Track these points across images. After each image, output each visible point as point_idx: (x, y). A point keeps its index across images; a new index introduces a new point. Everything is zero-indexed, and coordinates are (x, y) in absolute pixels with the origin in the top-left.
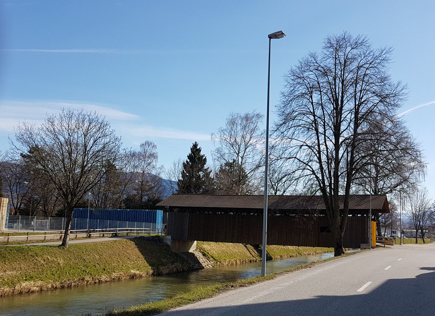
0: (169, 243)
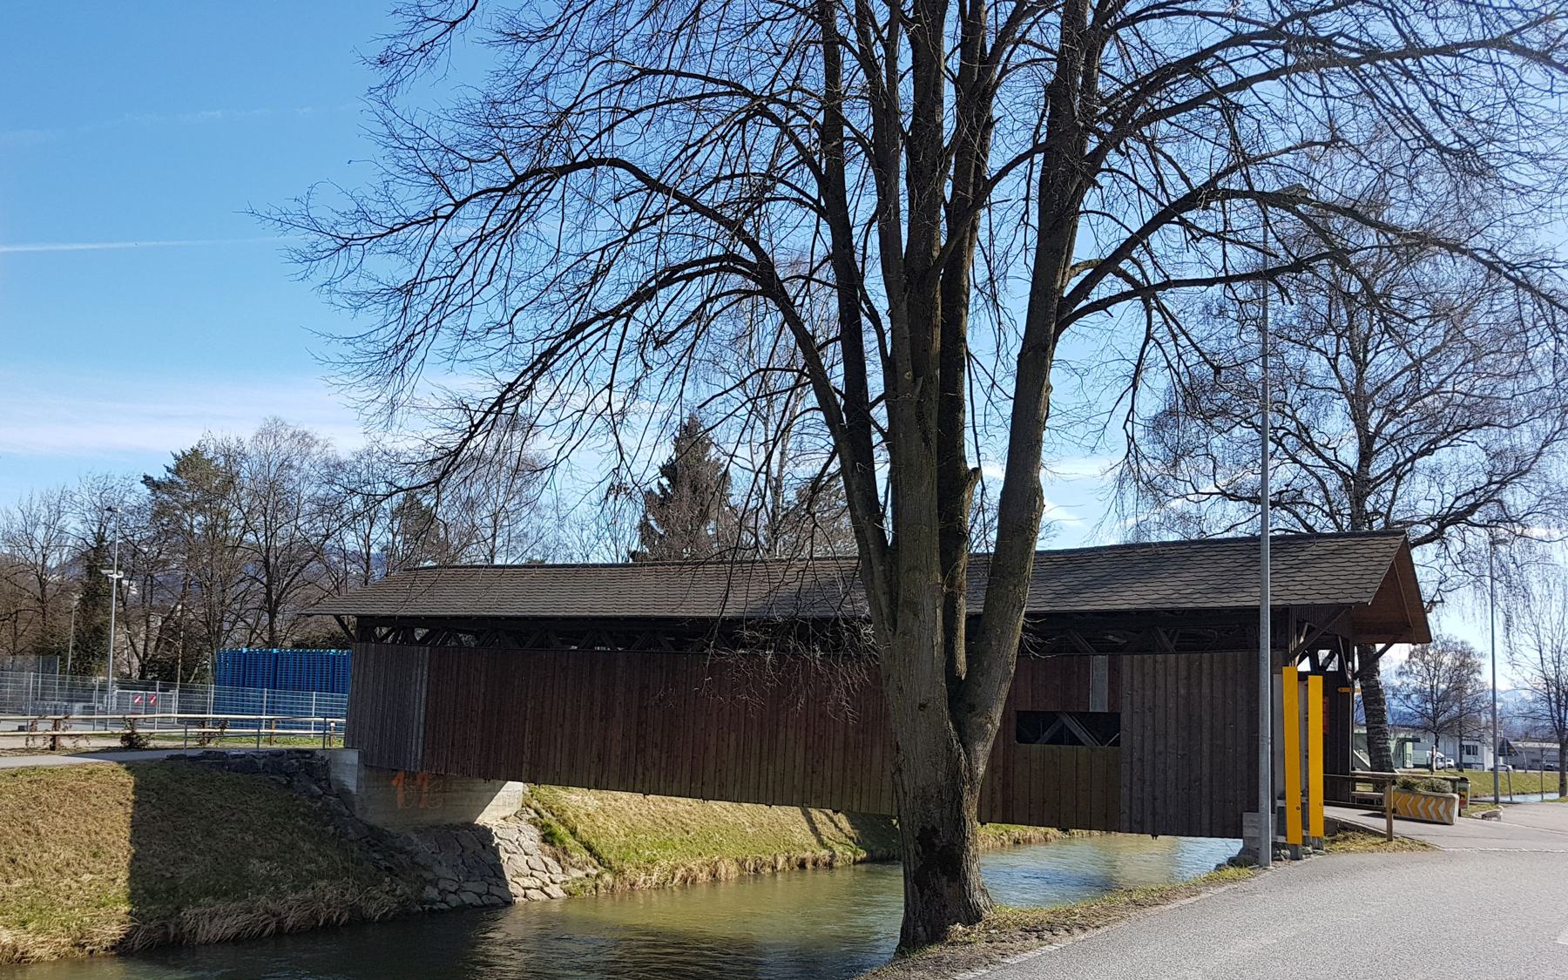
0: (351, 784)
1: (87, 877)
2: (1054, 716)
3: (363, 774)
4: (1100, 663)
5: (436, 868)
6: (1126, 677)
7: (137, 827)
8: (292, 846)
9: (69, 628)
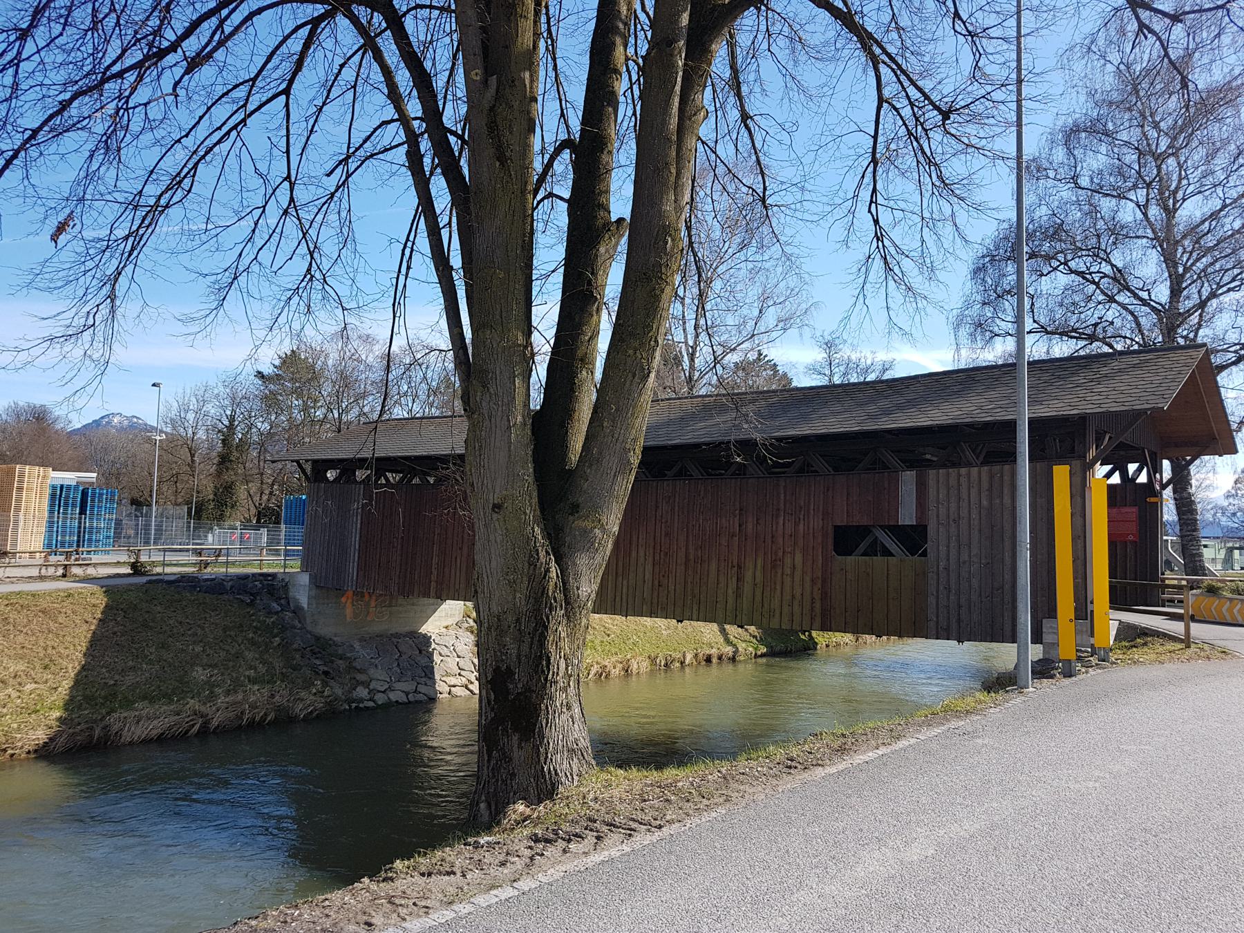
1: (30, 687)
2: (865, 531)
3: (313, 593)
4: (908, 479)
5: (372, 671)
6: (932, 492)
7: (95, 642)
8: (238, 656)
9: (208, 487)
